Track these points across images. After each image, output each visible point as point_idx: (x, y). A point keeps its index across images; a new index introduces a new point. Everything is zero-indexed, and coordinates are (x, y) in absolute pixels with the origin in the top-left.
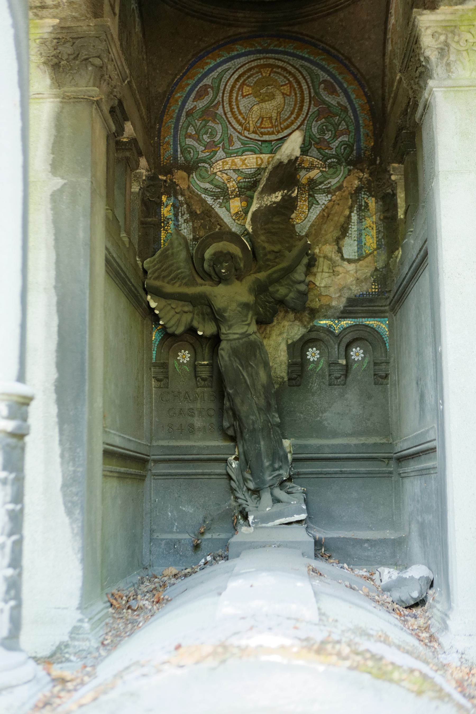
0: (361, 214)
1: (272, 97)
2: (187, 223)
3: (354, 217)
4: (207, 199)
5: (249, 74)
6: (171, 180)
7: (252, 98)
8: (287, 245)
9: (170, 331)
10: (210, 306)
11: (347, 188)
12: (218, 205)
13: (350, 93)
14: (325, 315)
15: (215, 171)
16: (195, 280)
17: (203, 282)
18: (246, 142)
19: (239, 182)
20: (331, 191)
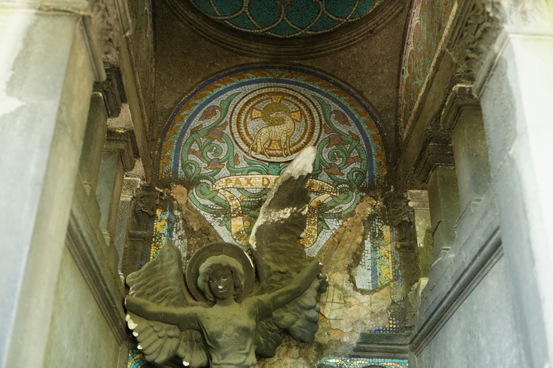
0: (375, 242)
1: (281, 121)
2: (182, 239)
3: (368, 245)
4: (206, 216)
5: (259, 99)
6: (168, 195)
7: (261, 121)
8: (295, 266)
9: (149, 358)
10: (201, 330)
11: (360, 214)
12: (218, 223)
13: (362, 124)
14: (335, 353)
15: (217, 188)
16: (185, 299)
17: (193, 302)
18: (252, 162)
19: (243, 201)
20: (343, 216)
